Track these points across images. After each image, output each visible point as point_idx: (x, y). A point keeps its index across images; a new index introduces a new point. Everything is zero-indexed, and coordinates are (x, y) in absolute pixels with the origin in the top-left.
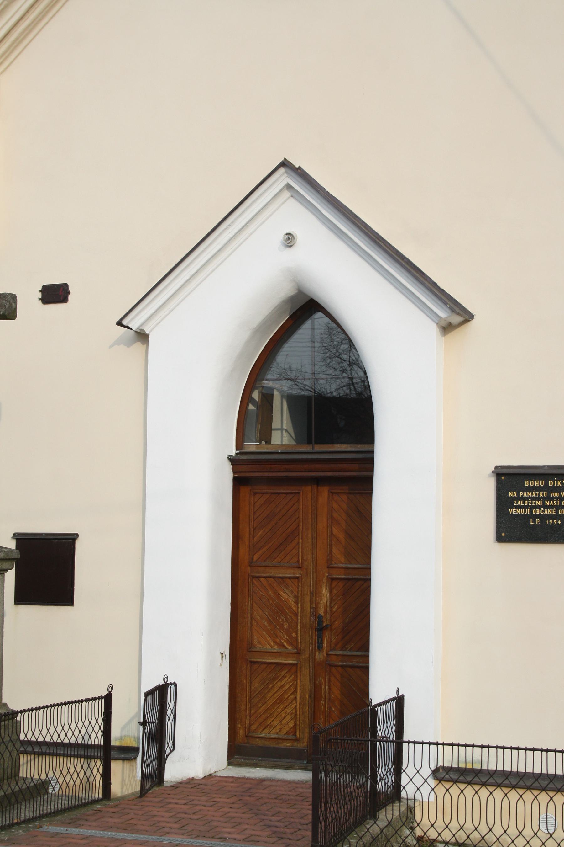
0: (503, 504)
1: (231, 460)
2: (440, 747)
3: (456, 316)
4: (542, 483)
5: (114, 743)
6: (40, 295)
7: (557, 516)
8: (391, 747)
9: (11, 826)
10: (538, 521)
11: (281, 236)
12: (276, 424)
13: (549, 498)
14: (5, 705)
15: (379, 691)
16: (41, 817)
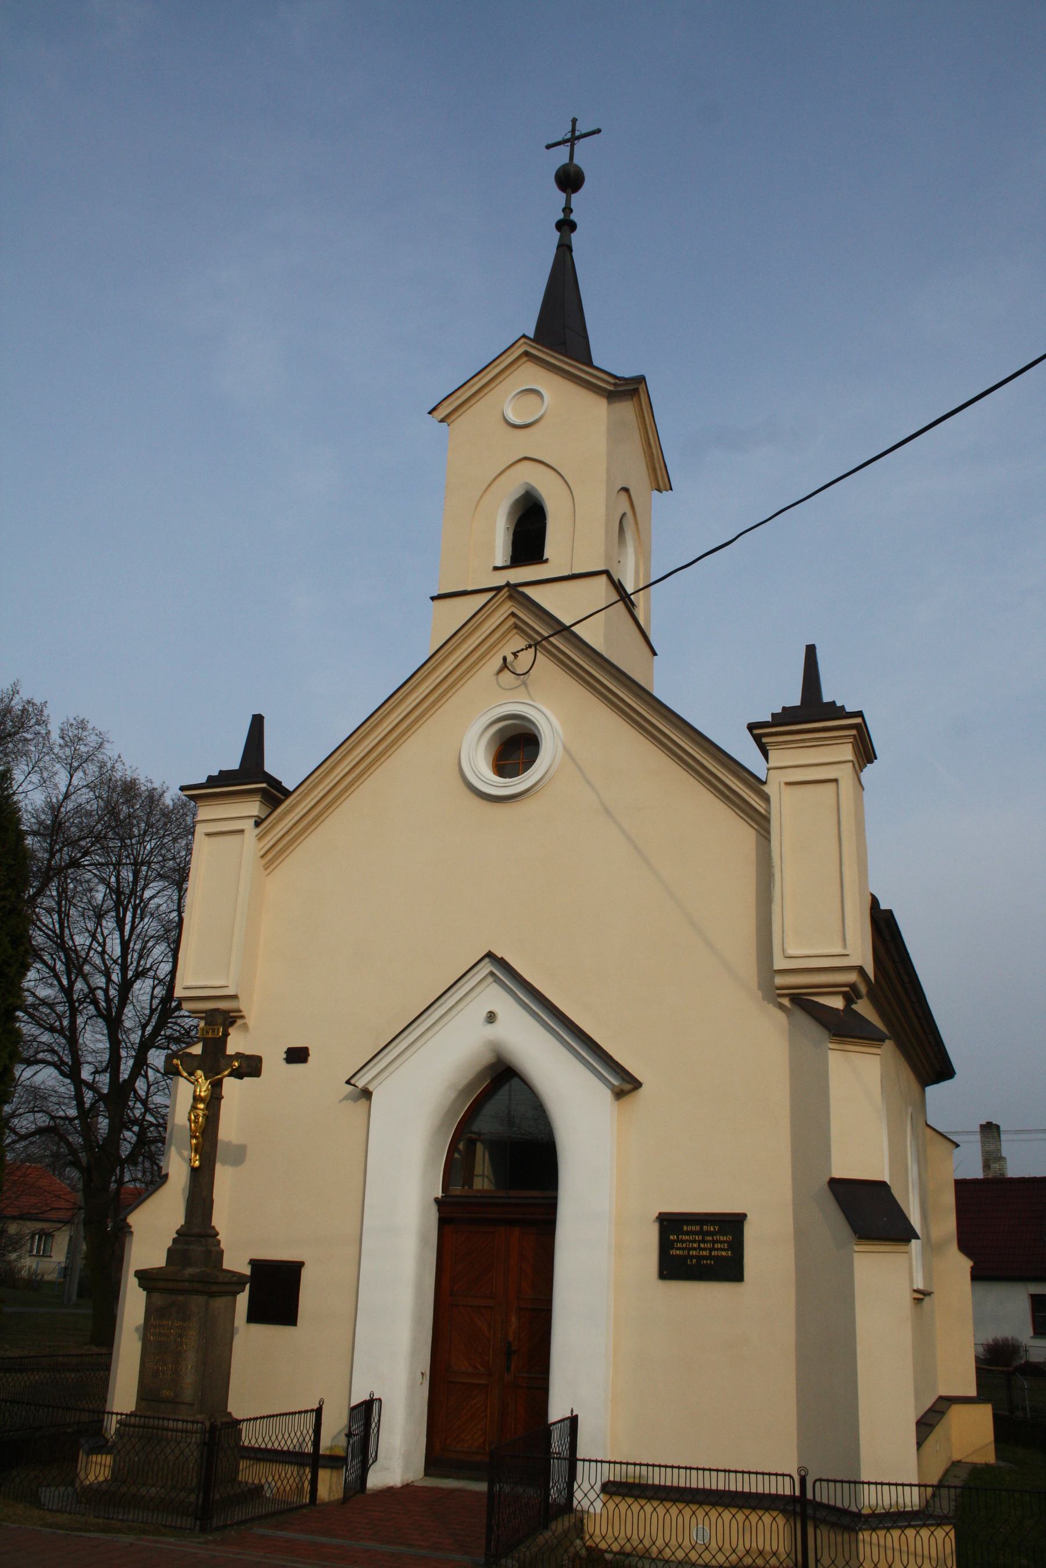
0: (665, 1246)
1: (436, 1200)
2: (599, 1464)
3: (626, 1085)
4: (698, 1228)
5: (322, 1451)
6: (285, 1056)
7: (710, 1257)
8: (565, 1464)
9: (225, 1526)
10: (694, 1261)
11: (484, 1014)
12: (478, 1170)
13: (704, 1241)
14: (230, 1413)
15: (557, 1411)
16: (253, 1519)
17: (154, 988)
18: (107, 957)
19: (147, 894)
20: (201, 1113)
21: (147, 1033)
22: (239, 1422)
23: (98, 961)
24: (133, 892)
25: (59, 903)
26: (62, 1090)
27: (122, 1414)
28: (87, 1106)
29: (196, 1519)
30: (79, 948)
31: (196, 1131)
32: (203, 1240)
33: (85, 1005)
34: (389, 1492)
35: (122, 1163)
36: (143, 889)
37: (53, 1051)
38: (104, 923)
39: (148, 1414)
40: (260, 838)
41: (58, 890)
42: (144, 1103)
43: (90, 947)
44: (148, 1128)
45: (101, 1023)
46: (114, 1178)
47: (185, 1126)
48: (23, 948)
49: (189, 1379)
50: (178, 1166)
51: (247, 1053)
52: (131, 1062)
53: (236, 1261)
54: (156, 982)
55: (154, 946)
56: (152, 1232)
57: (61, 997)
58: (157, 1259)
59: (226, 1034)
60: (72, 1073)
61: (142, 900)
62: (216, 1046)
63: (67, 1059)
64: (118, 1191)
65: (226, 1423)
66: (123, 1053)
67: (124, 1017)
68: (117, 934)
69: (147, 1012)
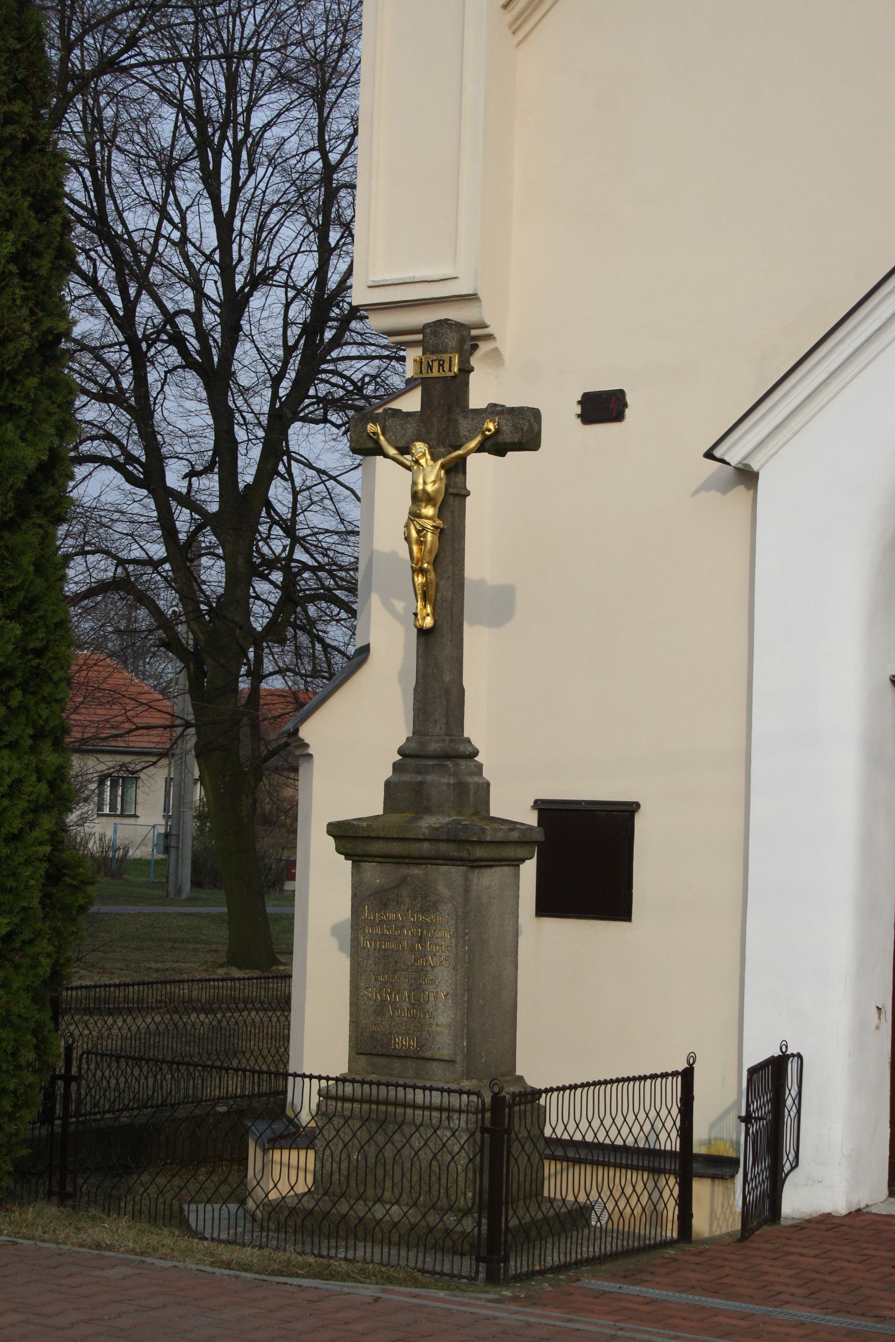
5: (697, 1149)
6: (578, 410)
9: (531, 1275)
14: (521, 1079)
16: (578, 1264)
17: (287, 306)
18: (191, 250)
19: (258, 119)
20: (428, 524)
21: (282, 393)
22: (537, 1093)
23: (173, 257)
24: (229, 118)
25: (90, 151)
26: (136, 508)
27: (328, 1079)
28: (182, 537)
29: (479, 1260)
30: (136, 237)
31: (421, 560)
32: (450, 764)
33: (159, 346)
34: (824, 1225)
35: (257, 639)
36: (249, 110)
37: (109, 437)
38: (179, 183)
39: (374, 1077)
41: (83, 120)
42: (290, 529)
43: (158, 235)
44: (299, 573)
45: (192, 379)
46: (244, 670)
47: (394, 554)
48: (57, 219)
49: (443, 1017)
50: (388, 629)
51: (509, 405)
52: (256, 452)
53: (513, 802)
54: (291, 294)
55: (280, 223)
56: (351, 751)
57: (115, 335)
58: (368, 803)
59: (466, 370)
60: (150, 477)
61: (248, 134)
62: (446, 396)
63: (138, 452)
64: (255, 689)
65: (520, 1094)
66: (240, 434)
67: (236, 366)
68: (206, 204)
69: (280, 352)
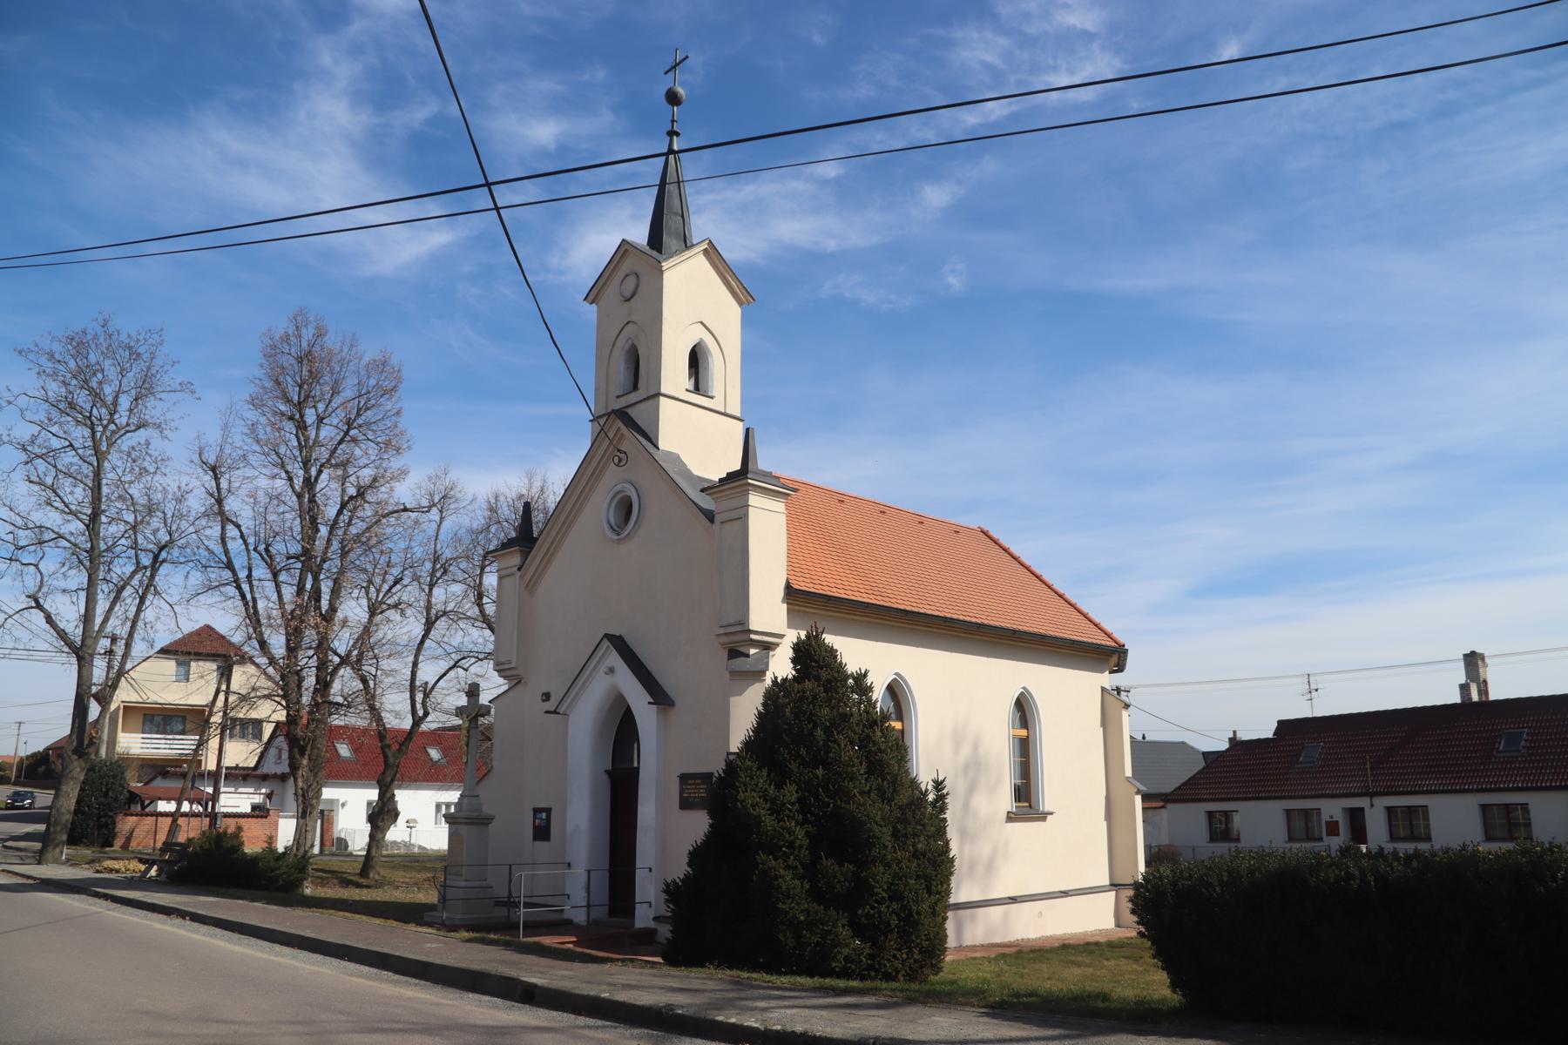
40: (522, 577)
